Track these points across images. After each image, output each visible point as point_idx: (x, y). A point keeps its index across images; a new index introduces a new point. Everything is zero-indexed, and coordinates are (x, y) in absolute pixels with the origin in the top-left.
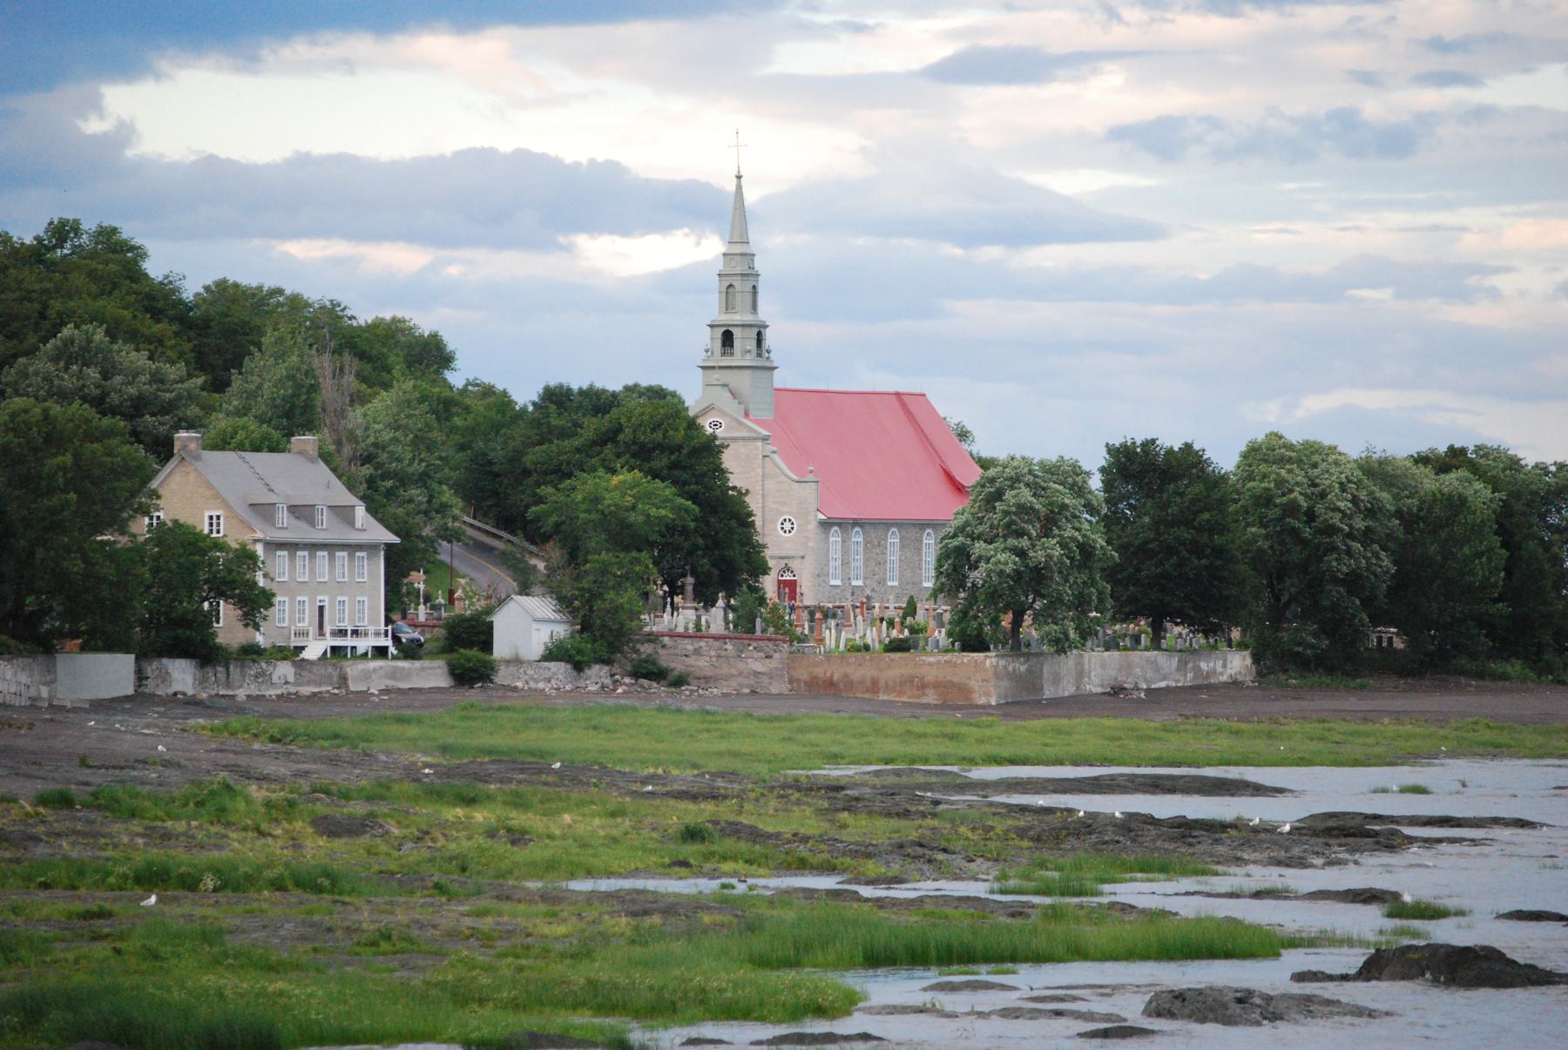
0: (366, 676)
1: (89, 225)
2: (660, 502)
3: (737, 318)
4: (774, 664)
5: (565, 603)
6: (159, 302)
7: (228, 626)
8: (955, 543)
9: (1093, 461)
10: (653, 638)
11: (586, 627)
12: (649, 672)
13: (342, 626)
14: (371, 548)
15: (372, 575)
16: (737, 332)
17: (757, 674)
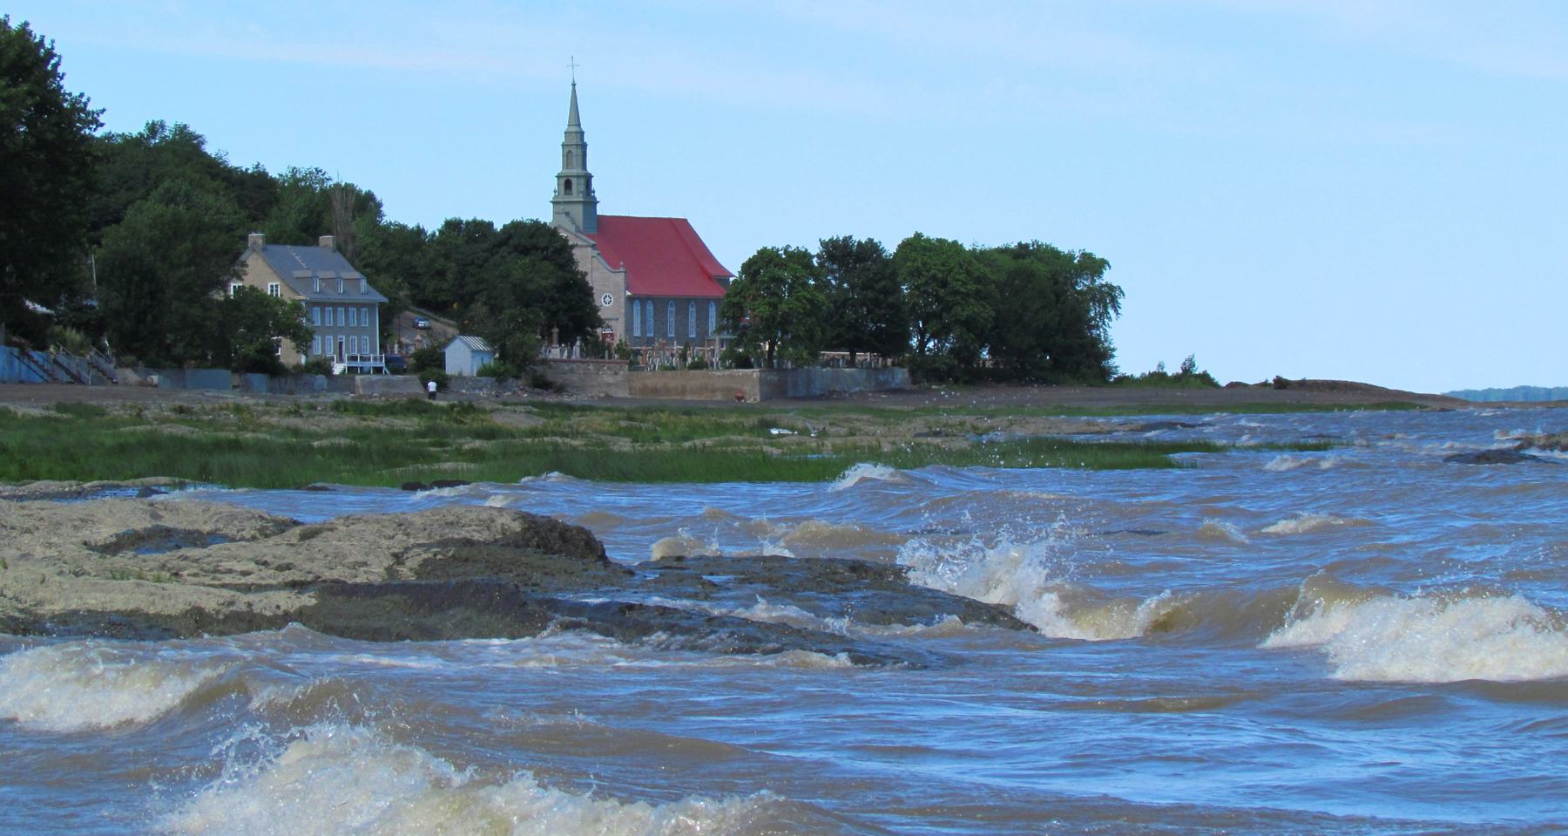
0: (371, 385)
1: (170, 125)
2: (545, 278)
3: (574, 171)
4: (619, 378)
5: (490, 339)
6: (216, 170)
7: (287, 353)
8: (735, 300)
9: (815, 249)
10: (545, 362)
11: (503, 357)
12: (542, 384)
13: (356, 353)
14: (370, 306)
15: (372, 322)
16: (574, 181)
17: (609, 385)
